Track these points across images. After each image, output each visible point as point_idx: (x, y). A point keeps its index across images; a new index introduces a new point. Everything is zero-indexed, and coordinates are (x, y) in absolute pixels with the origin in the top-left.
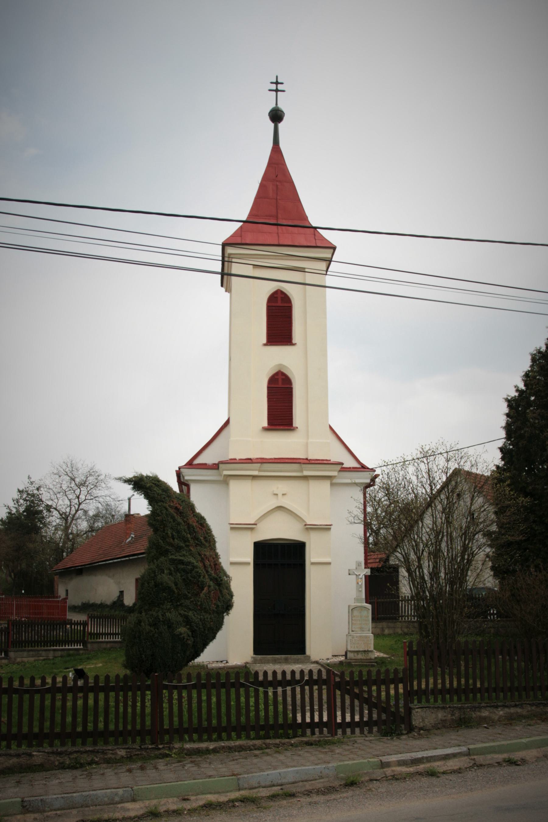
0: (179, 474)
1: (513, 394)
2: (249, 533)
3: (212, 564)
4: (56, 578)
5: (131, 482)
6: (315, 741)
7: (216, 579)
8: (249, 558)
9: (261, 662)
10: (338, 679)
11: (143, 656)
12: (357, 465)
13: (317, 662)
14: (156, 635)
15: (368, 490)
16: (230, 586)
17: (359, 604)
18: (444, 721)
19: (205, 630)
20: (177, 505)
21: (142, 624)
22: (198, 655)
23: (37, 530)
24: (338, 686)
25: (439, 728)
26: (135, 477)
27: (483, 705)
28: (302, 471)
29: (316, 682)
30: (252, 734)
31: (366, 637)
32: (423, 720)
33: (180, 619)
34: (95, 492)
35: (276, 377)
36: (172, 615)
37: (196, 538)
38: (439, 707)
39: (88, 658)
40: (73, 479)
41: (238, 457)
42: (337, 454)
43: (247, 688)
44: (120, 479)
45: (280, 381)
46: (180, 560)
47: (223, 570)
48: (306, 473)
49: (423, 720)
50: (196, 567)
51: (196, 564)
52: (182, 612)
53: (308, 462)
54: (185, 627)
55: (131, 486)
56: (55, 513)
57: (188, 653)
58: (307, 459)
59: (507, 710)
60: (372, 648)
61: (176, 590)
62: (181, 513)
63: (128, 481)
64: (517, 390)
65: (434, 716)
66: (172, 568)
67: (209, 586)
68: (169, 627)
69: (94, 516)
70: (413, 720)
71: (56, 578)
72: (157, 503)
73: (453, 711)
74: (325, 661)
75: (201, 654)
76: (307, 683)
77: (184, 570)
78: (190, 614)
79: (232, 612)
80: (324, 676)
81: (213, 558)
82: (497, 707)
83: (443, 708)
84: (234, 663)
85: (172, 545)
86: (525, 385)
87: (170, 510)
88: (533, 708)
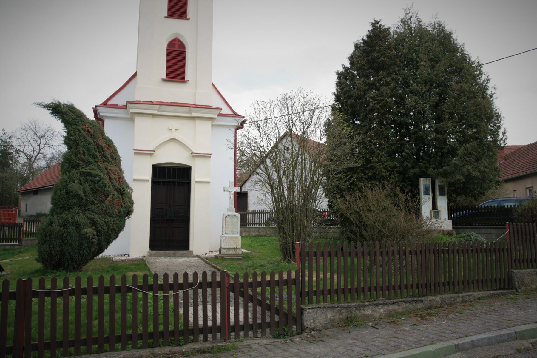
0: (96, 112)
1: (341, 70)
2: (148, 157)
3: (117, 177)
4: (20, 197)
5: (50, 107)
6: (208, 348)
7: (120, 189)
8: (148, 175)
9: (155, 256)
10: (232, 282)
11: (53, 252)
12: (232, 113)
13: (198, 256)
14: (65, 234)
15: (237, 131)
16: (131, 196)
17: (231, 213)
18: (333, 320)
19: (108, 230)
20: (89, 129)
21: (53, 225)
22: (103, 251)
23: (7, 165)
24: (232, 288)
25: (328, 328)
26: (53, 103)
27: (367, 303)
28: (191, 113)
29: (210, 285)
30: (140, 343)
31: (236, 238)
32: (314, 321)
33: (87, 221)
34: (51, 142)
35: (174, 42)
36: (80, 218)
37: (103, 156)
38: (328, 307)
39: (20, 252)
40: (36, 133)
41: (142, 100)
42: (217, 102)
43: (135, 293)
44: (39, 104)
45: (177, 46)
46: (89, 173)
47: (126, 183)
48: (194, 114)
49: (314, 321)
50: (103, 179)
51: (102, 176)
52: (89, 215)
53: (196, 106)
54: (90, 227)
55: (50, 111)
56: (22, 154)
57: (93, 249)
58: (195, 104)
59: (386, 307)
60: (239, 246)
61: (84, 197)
62: (91, 135)
63: (47, 107)
64: (344, 68)
65: (324, 316)
66: (82, 179)
67: (113, 195)
68: (77, 228)
69: (50, 158)
70: (305, 322)
71: (20, 197)
72: (71, 126)
73: (341, 311)
74: (204, 256)
75: (106, 250)
76: (201, 286)
77: (92, 181)
78: (96, 217)
79: (133, 216)
80: (218, 279)
81: (118, 173)
82: (378, 305)
83: (333, 308)
84: (134, 257)
85: (83, 161)
86: (350, 64)
87: (82, 131)
88: (408, 305)
